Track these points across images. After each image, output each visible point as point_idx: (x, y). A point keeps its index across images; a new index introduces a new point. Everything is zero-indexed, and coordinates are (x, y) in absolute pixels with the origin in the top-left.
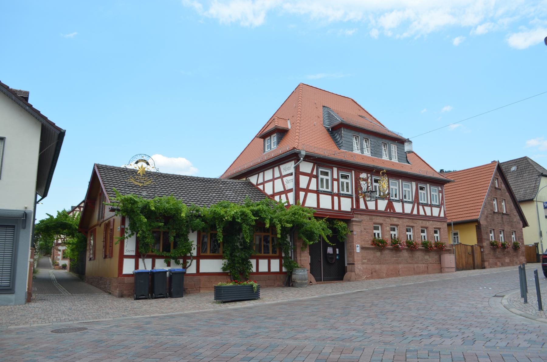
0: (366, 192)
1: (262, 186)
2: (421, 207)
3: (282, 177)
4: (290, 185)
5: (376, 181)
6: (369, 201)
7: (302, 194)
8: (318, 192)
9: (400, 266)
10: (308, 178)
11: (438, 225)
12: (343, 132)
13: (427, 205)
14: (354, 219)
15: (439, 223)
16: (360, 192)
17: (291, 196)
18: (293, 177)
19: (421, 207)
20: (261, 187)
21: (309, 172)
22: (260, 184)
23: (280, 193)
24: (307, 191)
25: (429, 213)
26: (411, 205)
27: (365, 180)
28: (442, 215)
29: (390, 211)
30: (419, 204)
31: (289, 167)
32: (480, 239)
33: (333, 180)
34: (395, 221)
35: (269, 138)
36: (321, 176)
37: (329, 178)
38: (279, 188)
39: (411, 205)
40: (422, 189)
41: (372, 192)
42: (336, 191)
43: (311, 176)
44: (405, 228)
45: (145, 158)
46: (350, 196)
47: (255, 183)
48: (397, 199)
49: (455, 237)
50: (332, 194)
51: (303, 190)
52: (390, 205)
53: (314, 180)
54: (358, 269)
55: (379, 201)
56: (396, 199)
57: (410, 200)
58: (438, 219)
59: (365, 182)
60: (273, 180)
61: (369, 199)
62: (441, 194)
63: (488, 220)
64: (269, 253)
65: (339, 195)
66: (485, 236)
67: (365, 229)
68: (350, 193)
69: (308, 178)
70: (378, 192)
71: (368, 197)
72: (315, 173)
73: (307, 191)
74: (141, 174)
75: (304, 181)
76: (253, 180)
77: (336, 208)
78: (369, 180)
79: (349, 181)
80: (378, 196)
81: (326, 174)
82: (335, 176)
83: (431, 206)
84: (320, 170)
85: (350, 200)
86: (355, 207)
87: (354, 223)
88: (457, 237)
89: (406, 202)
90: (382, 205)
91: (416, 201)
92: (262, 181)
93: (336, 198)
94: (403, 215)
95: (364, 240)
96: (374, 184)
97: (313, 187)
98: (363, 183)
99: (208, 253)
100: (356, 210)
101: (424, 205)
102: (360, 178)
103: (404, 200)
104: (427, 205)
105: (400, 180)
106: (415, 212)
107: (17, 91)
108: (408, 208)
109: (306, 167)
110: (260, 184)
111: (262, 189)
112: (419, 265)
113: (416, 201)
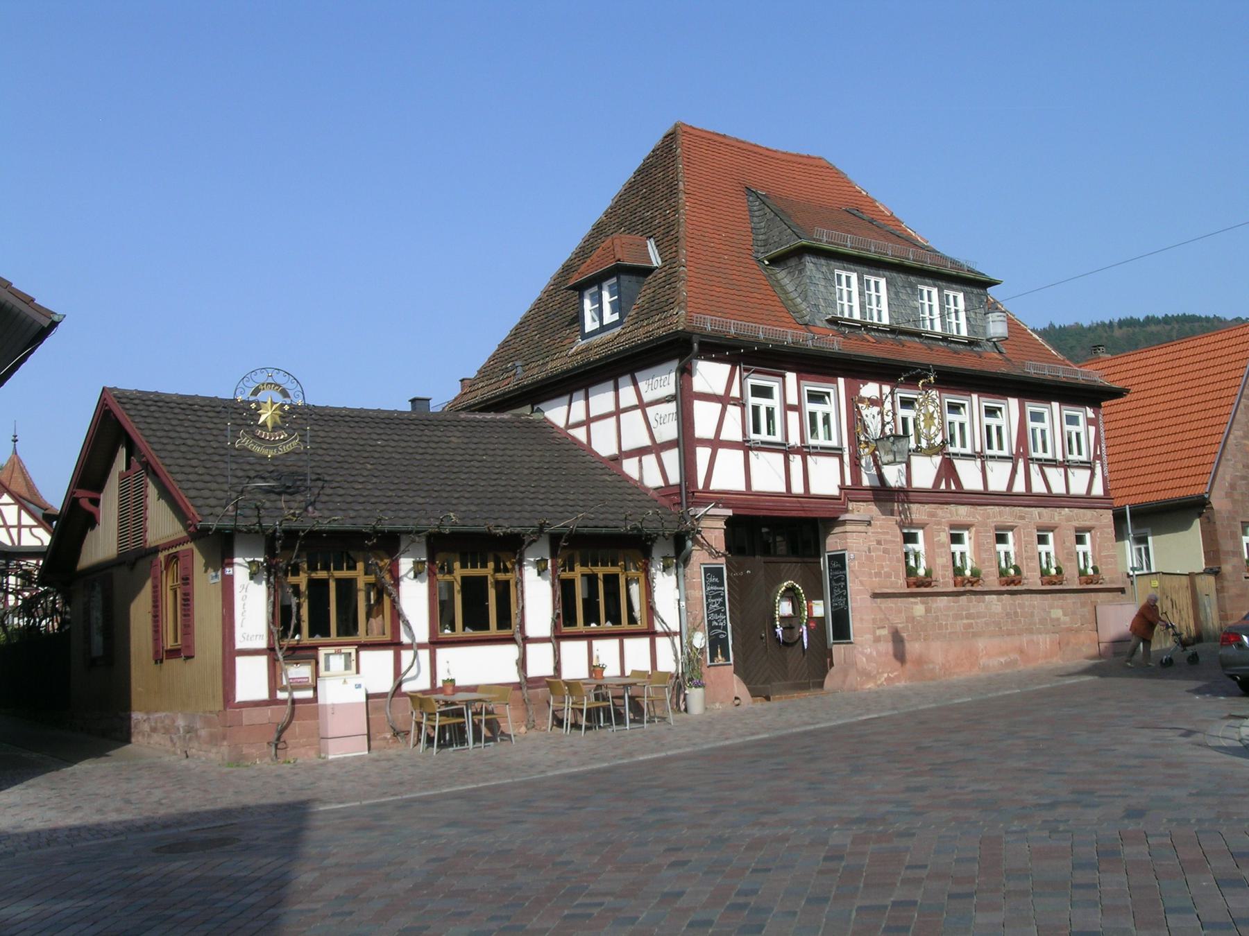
0: (880, 439)
1: (584, 429)
2: (1034, 468)
3: (642, 406)
4: (668, 430)
5: (907, 403)
6: (888, 464)
7: (703, 454)
8: (746, 447)
9: (981, 644)
10: (719, 406)
11: (1086, 517)
12: (810, 263)
13: (1053, 463)
14: (847, 517)
15: (1089, 512)
16: (862, 438)
17: (672, 458)
18: (672, 407)
19: (1034, 468)
20: (580, 434)
21: (720, 391)
22: (578, 425)
23: (640, 452)
24: (716, 444)
25: (1058, 488)
26: (1008, 466)
27: (878, 402)
28: (1098, 490)
29: (948, 485)
30: (1029, 461)
31: (660, 383)
32: (1213, 552)
33: (788, 408)
34: (962, 513)
35: (595, 289)
36: (752, 401)
37: (775, 403)
38: (635, 435)
39: (1008, 466)
40: (1038, 417)
41: (897, 437)
42: (794, 440)
43: (724, 400)
44: (992, 534)
45: (280, 379)
46: (835, 452)
47: (561, 423)
48: (968, 450)
49: (1140, 550)
50: (786, 450)
51: (704, 442)
52: (948, 470)
53: (733, 412)
54: (863, 654)
55: (915, 460)
56: (963, 451)
57: (1005, 453)
58: (1086, 502)
59: (876, 409)
60: (618, 412)
61: (890, 458)
62: (1092, 429)
63: (1237, 496)
64: (487, 627)
65: (805, 451)
66: (1226, 545)
67: (879, 543)
68: (834, 443)
69: (718, 407)
70: (912, 439)
71: (887, 453)
72: (735, 392)
73: (716, 444)
74: (269, 425)
75: (705, 418)
76: (556, 414)
77: (797, 488)
78: (888, 406)
79: (829, 407)
80: (913, 445)
81: (765, 392)
82: (792, 399)
83: (1066, 465)
84: (750, 382)
85: (836, 461)
86: (848, 482)
87: (848, 528)
88: (1147, 549)
89: (992, 457)
90: (925, 472)
91: (1021, 454)
92: (582, 417)
93: (796, 461)
94: (985, 498)
95: (878, 574)
96: (902, 413)
97: (732, 431)
98: (870, 414)
99: (460, 633)
100: (851, 492)
101: (1043, 463)
102: (862, 400)
103: (989, 452)
104: (1053, 463)
105: (975, 397)
106: (1019, 487)
107: (1141, 676)
108: (998, 478)
109: (711, 375)
110: (578, 425)
111: (583, 439)
112: (1035, 638)
113: (1021, 454)
